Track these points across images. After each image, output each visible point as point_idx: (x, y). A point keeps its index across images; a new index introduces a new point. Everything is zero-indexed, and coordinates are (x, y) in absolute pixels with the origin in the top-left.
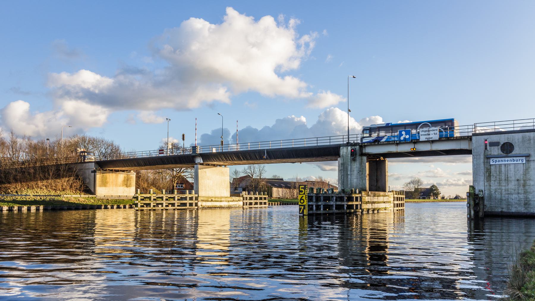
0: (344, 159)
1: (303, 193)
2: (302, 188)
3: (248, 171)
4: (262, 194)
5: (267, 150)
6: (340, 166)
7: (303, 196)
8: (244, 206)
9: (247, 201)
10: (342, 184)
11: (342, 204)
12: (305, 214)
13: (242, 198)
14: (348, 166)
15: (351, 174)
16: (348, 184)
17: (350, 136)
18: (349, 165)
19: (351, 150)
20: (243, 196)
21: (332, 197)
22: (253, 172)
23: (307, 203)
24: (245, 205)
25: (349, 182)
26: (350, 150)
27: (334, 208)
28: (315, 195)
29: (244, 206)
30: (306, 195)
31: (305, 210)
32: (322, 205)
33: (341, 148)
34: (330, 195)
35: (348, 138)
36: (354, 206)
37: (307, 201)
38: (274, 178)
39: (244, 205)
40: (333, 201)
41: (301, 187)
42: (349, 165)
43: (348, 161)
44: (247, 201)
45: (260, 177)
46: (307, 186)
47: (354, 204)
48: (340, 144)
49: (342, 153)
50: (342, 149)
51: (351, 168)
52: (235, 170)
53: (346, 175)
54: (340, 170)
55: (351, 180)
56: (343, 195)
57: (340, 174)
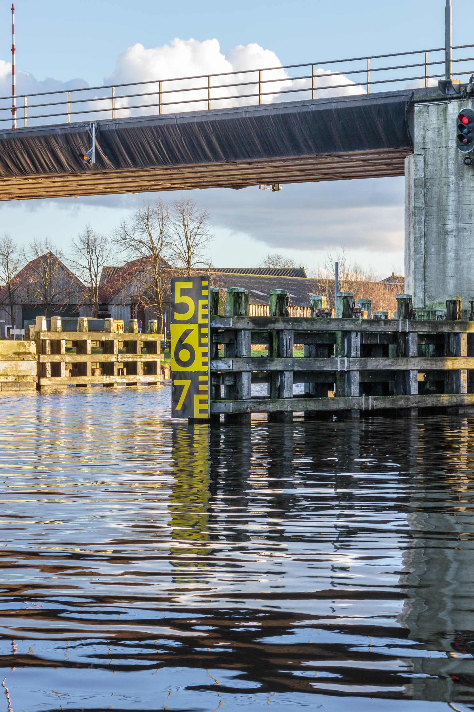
0: (430, 161)
1: (188, 315)
2: (184, 292)
3: (137, 236)
4: (136, 327)
5: (99, 124)
6: (412, 195)
7: (186, 334)
8: (43, 381)
9: (57, 358)
10: (420, 277)
11: (399, 368)
12: (197, 415)
13: (33, 348)
14: (448, 193)
15: (460, 230)
16: (444, 274)
17: (454, 54)
18: (452, 187)
19: (461, 117)
20: (38, 334)
21: (346, 334)
22: (155, 236)
23: (204, 364)
24: (48, 375)
25: (450, 270)
26: (456, 117)
27: (355, 389)
28: (251, 326)
29: (43, 381)
30: (201, 326)
31: (197, 398)
32: (287, 374)
33: (417, 108)
34: (332, 327)
35: (448, 61)
36: (458, 379)
37: (204, 354)
38: (272, 267)
39: (44, 376)
40: (348, 355)
41: (180, 286)
42: (452, 187)
43: (447, 169)
44: (57, 358)
45: (188, 262)
46: (205, 283)
47: (462, 367)
48: (413, 92)
49: (422, 133)
50: (420, 111)
51: (459, 202)
52: (83, 233)
53: (439, 233)
54: (414, 214)
55: (458, 258)
56: (403, 327)
57: (412, 230)
